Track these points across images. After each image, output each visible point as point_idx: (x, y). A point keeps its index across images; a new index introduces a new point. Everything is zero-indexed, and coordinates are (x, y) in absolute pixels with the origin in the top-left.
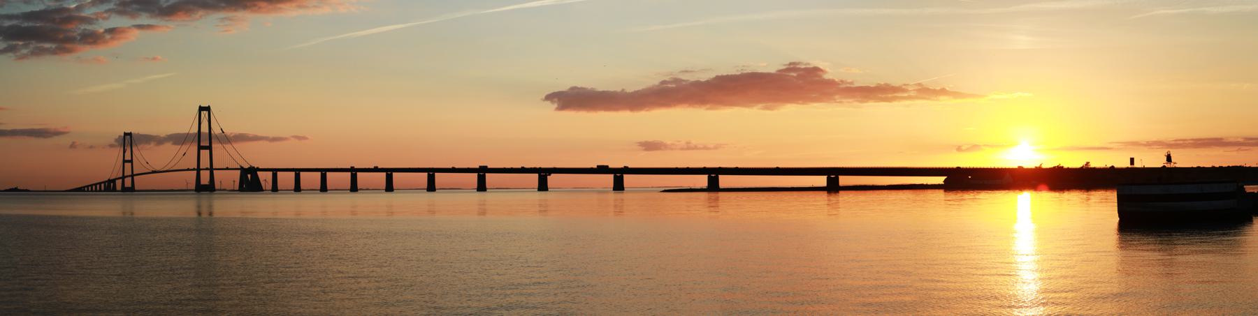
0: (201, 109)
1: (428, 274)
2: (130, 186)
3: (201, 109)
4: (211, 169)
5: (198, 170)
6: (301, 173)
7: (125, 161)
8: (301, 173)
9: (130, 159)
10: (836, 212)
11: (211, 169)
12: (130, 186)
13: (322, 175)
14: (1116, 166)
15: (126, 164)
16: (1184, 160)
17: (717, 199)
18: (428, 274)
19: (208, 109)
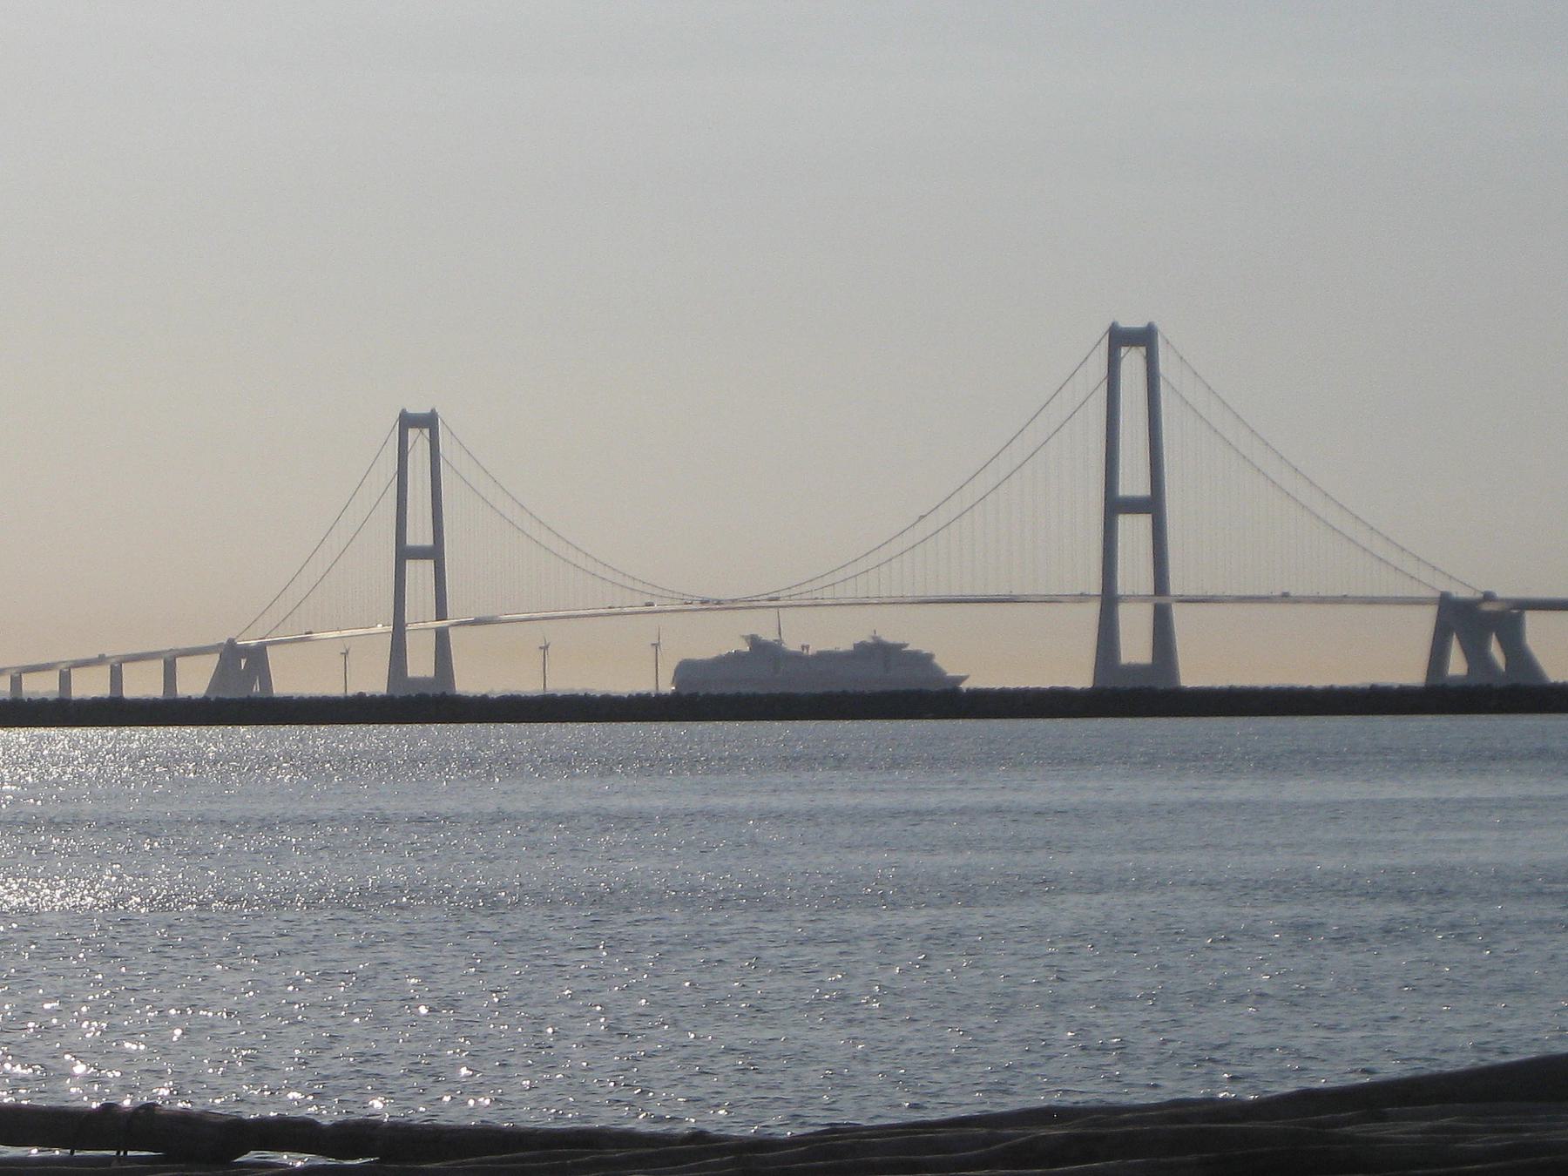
0: (407, 422)
5: (1109, 600)
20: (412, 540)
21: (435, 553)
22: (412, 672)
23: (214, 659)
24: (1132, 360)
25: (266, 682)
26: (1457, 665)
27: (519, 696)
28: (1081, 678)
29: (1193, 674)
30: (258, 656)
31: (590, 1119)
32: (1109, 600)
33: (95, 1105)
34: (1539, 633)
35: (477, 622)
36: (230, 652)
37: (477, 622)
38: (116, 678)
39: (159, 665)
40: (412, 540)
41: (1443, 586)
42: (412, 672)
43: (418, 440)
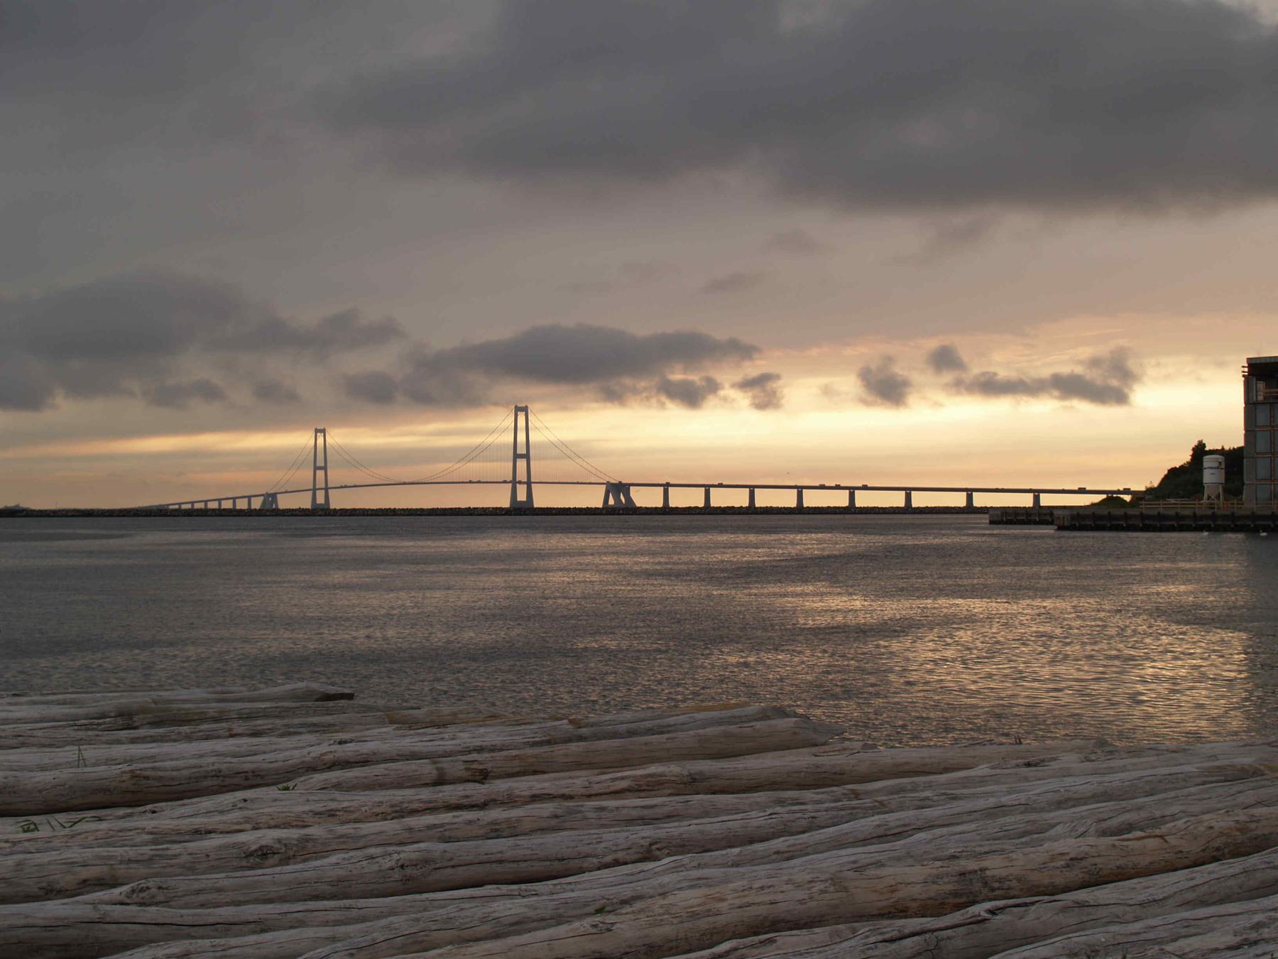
9: (323, 465)
12: (525, 499)
22: (318, 502)
25: (277, 505)
26: (611, 502)
34: (634, 493)
42: (318, 502)
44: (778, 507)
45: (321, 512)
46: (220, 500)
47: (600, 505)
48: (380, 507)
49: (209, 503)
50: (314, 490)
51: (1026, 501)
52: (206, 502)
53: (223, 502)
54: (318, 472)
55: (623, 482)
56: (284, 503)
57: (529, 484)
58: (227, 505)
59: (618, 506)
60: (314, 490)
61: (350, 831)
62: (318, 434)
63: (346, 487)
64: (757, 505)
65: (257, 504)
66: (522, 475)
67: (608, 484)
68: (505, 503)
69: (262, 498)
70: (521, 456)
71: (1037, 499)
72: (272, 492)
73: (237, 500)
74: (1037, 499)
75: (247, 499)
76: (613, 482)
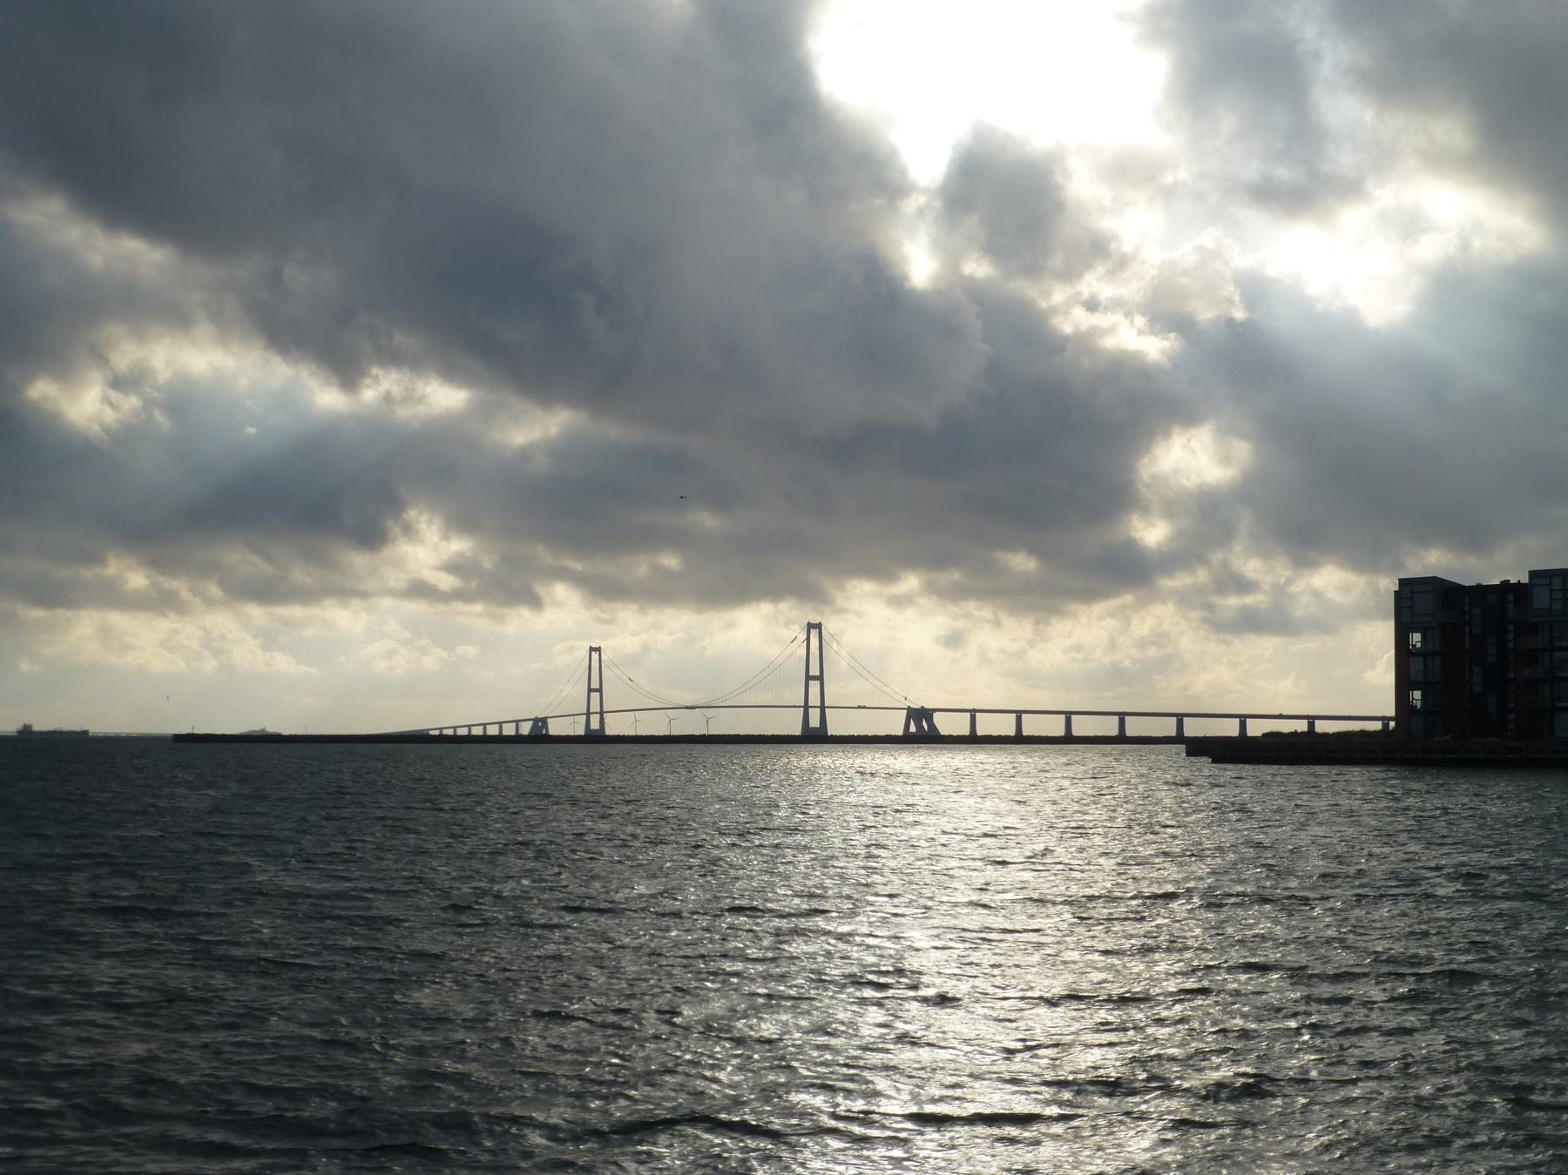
0: (592, 649)
1: (1130, 807)
2: (598, 728)
3: (592, 649)
4: (823, 708)
5: (806, 707)
6: (1185, 719)
7: (590, 690)
8: (1185, 719)
9: (598, 687)
10: (862, 1011)
11: (823, 708)
12: (598, 728)
13: (1178, 720)
14: (36, 728)
15: (592, 694)
16: (1321, 727)
17: (1384, 618)
18: (1130, 807)
19: (598, 650)
20: (812, 673)
21: (600, 690)
22: (592, 728)
23: (531, 722)
24: (814, 633)
25: (547, 730)
26: (913, 729)
27: (61, 733)
28: (797, 731)
29: (609, 731)
30: (544, 720)
31: (866, 1074)
32: (806, 707)
33: (754, 1123)
34: (938, 718)
35: (860, 707)
36: (536, 720)
37: (860, 707)
38: (470, 730)
39: (514, 724)
40: (812, 673)
41: (908, 704)
42: (592, 728)
43: (595, 656)
44: (991, 736)
45: (595, 738)
46: (470, 727)
47: (901, 733)
48: (1326, 731)
49: (473, 728)
50: (588, 714)
51: (1230, 729)
52: (455, 728)
53: (473, 728)
54: (592, 694)
55: (926, 707)
56: (555, 729)
57: (602, 713)
58: (477, 731)
59: (932, 734)
60: (588, 714)
61: (40, 1099)
62: (593, 653)
63: (865, 707)
64: (1025, 733)
65: (525, 729)
66: (595, 707)
67: (909, 709)
68: (581, 731)
69: (531, 722)
70: (814, 678)
71: (1243, 726)
72: (542, 716)
73: (504, 725)
74: (1243, 726)
75: (514, 724)
76: (913, 706)
